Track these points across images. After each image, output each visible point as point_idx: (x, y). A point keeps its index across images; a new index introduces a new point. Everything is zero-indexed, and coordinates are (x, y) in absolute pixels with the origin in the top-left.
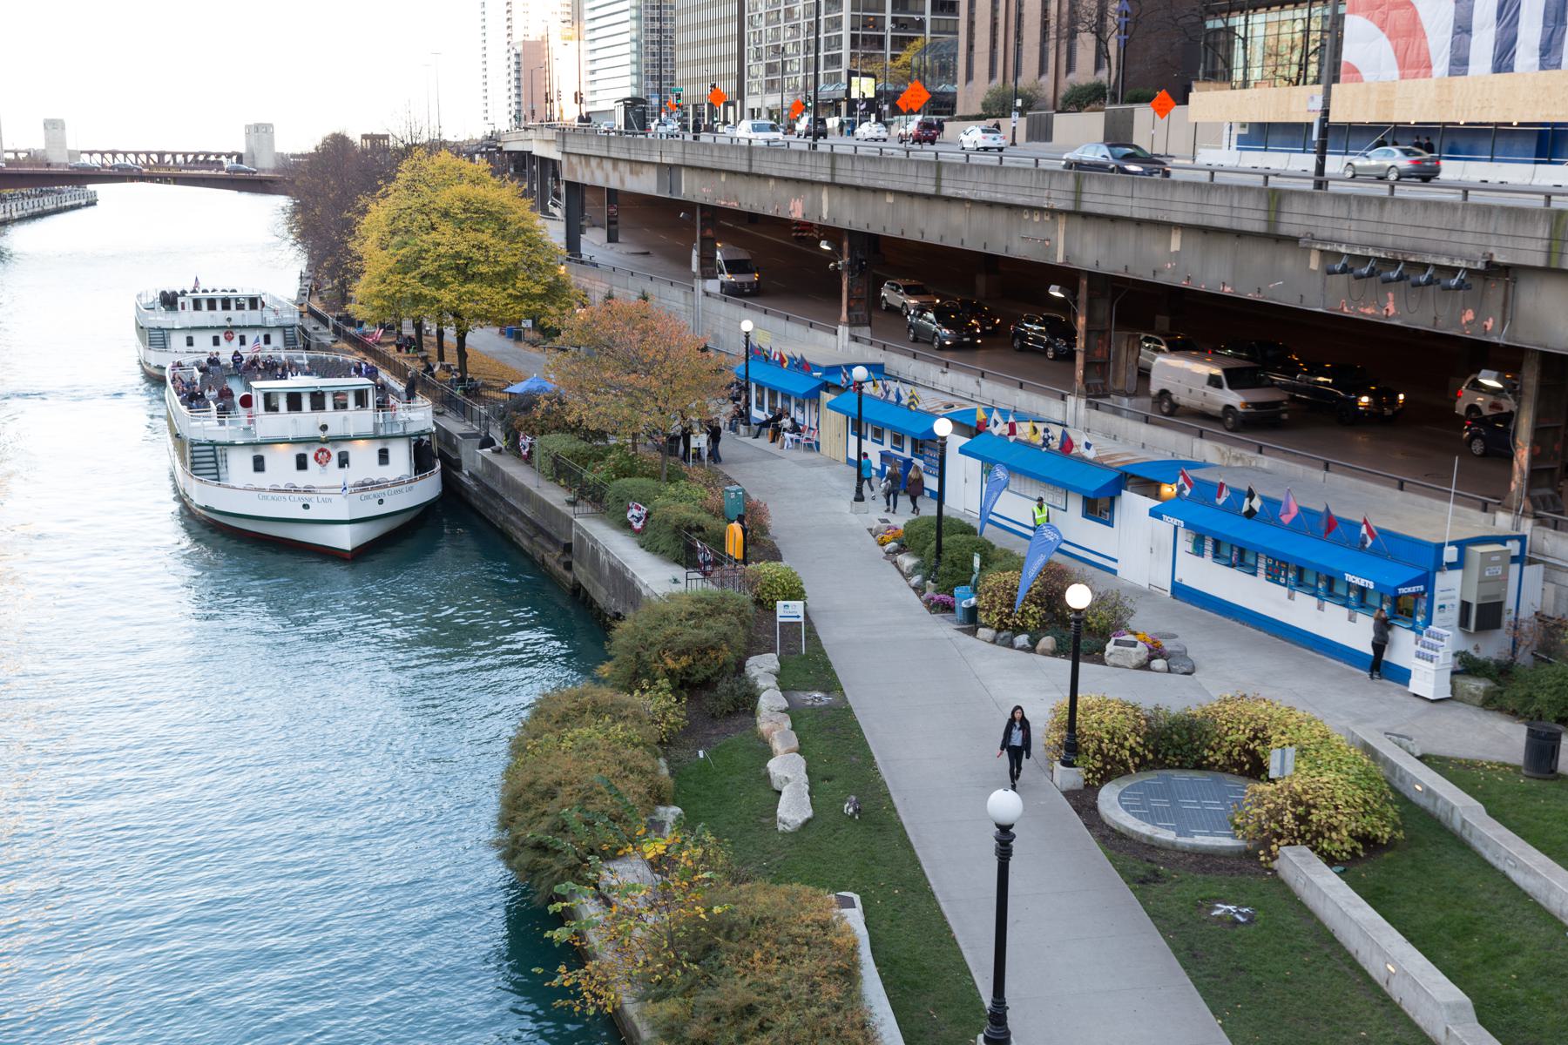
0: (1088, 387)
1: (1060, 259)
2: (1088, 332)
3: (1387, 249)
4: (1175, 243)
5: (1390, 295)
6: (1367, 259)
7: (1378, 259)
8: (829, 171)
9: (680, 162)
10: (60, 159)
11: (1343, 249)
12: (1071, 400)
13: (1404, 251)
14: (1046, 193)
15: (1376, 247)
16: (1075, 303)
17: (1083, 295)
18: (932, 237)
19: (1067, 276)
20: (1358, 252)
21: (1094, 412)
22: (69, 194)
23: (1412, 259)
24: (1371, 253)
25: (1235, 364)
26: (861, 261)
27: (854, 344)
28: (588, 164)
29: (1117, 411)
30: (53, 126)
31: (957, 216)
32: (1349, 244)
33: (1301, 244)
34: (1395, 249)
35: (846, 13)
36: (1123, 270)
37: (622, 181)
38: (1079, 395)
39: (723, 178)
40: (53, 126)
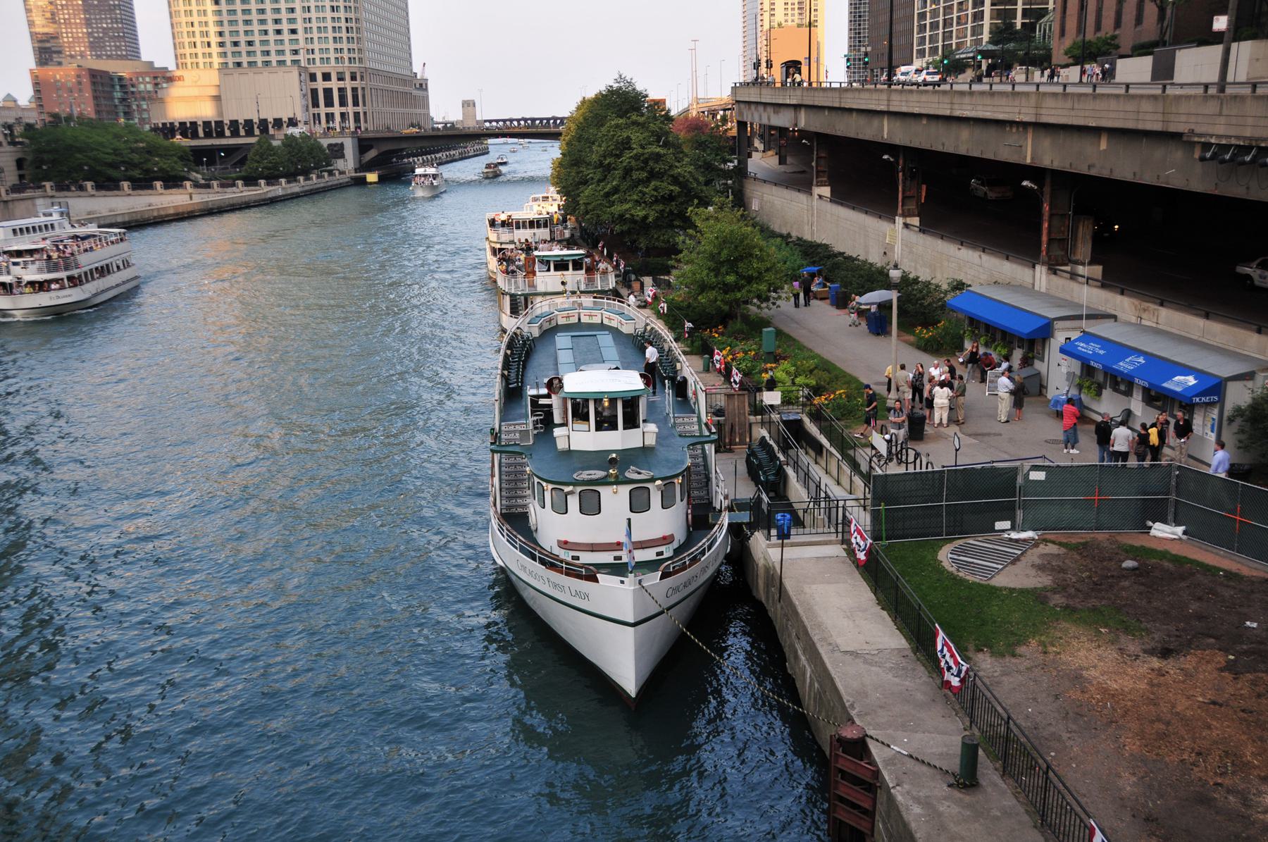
0: (1049, 257)
1: (1028, 161)
2: (1051, 216)
3: (1245, 138)
4: (1103, 145)
5: (885, 136)
6: (1229, 146)
7: (1238, 146)
8: (886, 103)
9: (800, 102)
10: (471, 125)
11: (1213, 141)
12: (1038, 267)
13: (1257, 139)
14: (1017, 110)
15: (1237, 138)
16: (1042, 193)
17: (1047, 189)
18: (949, 148)
19: (1036, 173)
20: (1224, 142)
21: (1053, 277)
22: (471, 147)
23: (1263, 145)
24: (1233, 141)
25: (556, 216)
26: (912, 168)
27: (906, 231)
28: (750, 108)
29: (1073, 276)
30: (468, 105)
31: (965, 133)
32: (1218, 136)
33: (1185, 138)
34: (1250, 139)
35: (987, 8)
36: (1068, 166)
37: (769, 119)
38: (1043, 264)
39: (924, 122)
40: (468, 105)
